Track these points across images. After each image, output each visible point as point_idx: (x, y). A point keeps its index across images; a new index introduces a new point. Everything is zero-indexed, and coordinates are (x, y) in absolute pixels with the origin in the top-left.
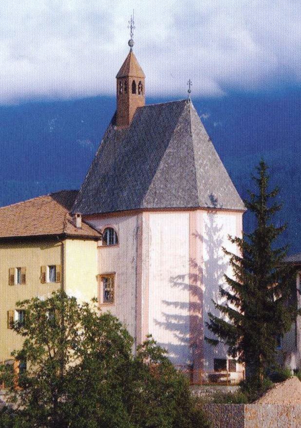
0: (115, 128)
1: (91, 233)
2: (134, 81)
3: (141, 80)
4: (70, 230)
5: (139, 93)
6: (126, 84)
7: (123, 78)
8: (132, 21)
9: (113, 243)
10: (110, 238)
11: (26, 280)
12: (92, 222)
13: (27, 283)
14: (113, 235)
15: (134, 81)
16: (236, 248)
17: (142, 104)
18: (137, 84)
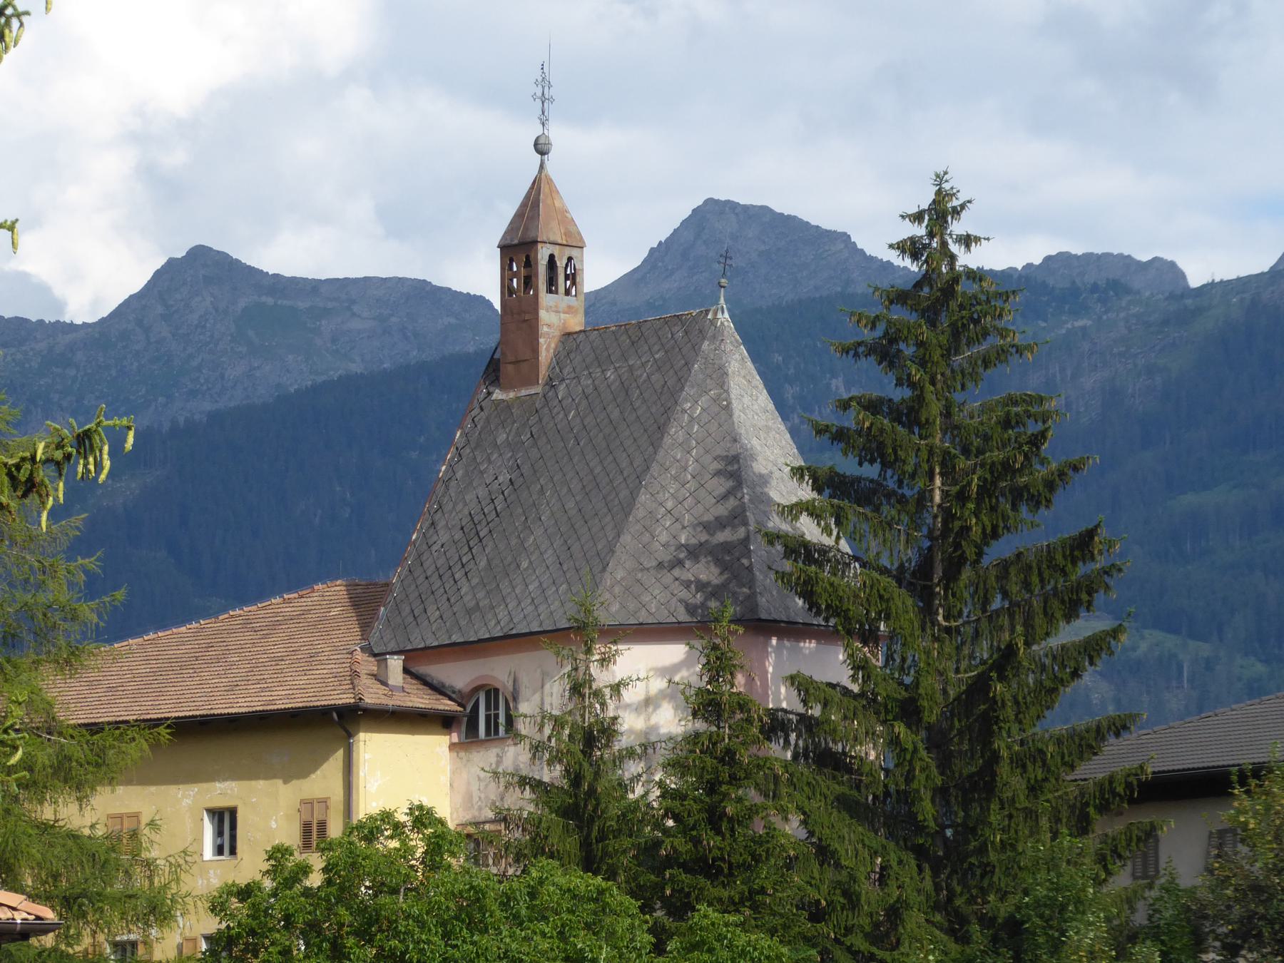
0: (498, 395)
1: (420, 699)
2: (552, 257)
3: (574, 253)
4: (373, 696)
5: (567, 292)
6: (529, 263)
7: (518, 250)
8: (544, 82)
9: (497, 732)
10: (488, 718)
11: (239, 849)
12: (423, 669)
13: (239, 854)
14: (497, 708)
15: (552, 257)
16: (445, 779)
17: (576, 323)
18: (561, 263)
